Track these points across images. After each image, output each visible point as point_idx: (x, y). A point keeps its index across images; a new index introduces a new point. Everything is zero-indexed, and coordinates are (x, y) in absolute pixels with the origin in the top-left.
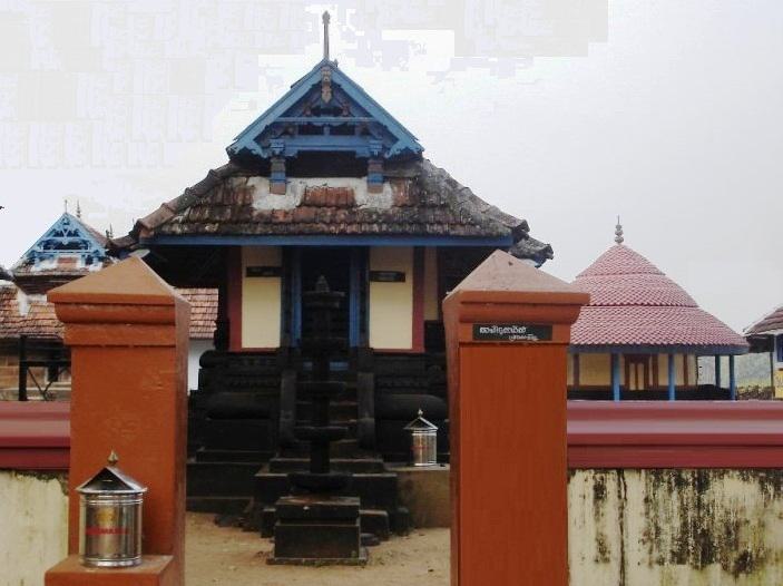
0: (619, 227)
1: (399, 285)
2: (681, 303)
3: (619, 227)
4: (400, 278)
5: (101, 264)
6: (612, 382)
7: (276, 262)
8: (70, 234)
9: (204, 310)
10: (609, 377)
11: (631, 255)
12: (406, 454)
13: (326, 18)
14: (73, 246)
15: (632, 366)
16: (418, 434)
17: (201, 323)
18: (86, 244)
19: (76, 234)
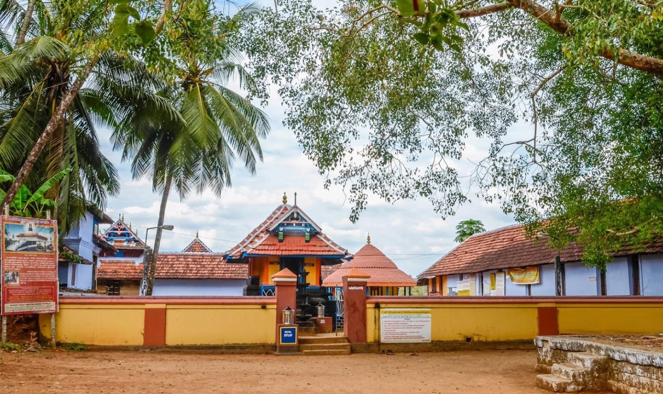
0: (369, 237)
1: (312, 267)
2: (389, 266)
3: (369, 237)
4: (313, 265)
5: (135, 244)
6: (180, 350)
7: (278, 260)
8: (121, 230)
9: (183, 265)
10: (538, 277)
11: (373, 248)
12: (316, 314)
13: (295, 194)
14: (123, 235)
15: (373, 291)
16: (319, 308)
17: (182, 271)
18: (129, 235)
19: (124, 229)
